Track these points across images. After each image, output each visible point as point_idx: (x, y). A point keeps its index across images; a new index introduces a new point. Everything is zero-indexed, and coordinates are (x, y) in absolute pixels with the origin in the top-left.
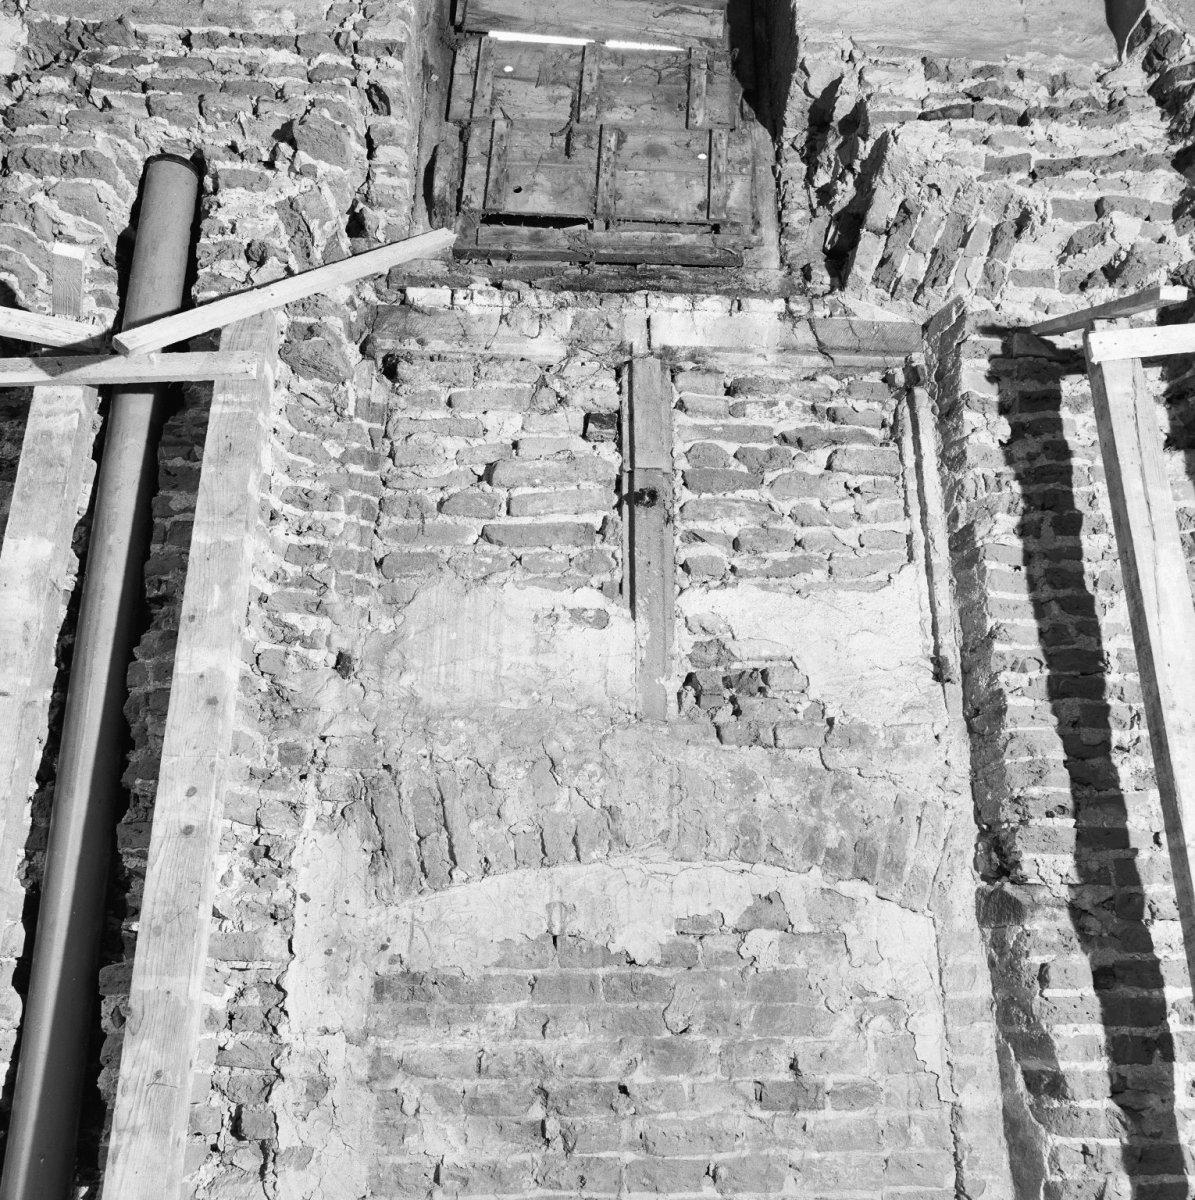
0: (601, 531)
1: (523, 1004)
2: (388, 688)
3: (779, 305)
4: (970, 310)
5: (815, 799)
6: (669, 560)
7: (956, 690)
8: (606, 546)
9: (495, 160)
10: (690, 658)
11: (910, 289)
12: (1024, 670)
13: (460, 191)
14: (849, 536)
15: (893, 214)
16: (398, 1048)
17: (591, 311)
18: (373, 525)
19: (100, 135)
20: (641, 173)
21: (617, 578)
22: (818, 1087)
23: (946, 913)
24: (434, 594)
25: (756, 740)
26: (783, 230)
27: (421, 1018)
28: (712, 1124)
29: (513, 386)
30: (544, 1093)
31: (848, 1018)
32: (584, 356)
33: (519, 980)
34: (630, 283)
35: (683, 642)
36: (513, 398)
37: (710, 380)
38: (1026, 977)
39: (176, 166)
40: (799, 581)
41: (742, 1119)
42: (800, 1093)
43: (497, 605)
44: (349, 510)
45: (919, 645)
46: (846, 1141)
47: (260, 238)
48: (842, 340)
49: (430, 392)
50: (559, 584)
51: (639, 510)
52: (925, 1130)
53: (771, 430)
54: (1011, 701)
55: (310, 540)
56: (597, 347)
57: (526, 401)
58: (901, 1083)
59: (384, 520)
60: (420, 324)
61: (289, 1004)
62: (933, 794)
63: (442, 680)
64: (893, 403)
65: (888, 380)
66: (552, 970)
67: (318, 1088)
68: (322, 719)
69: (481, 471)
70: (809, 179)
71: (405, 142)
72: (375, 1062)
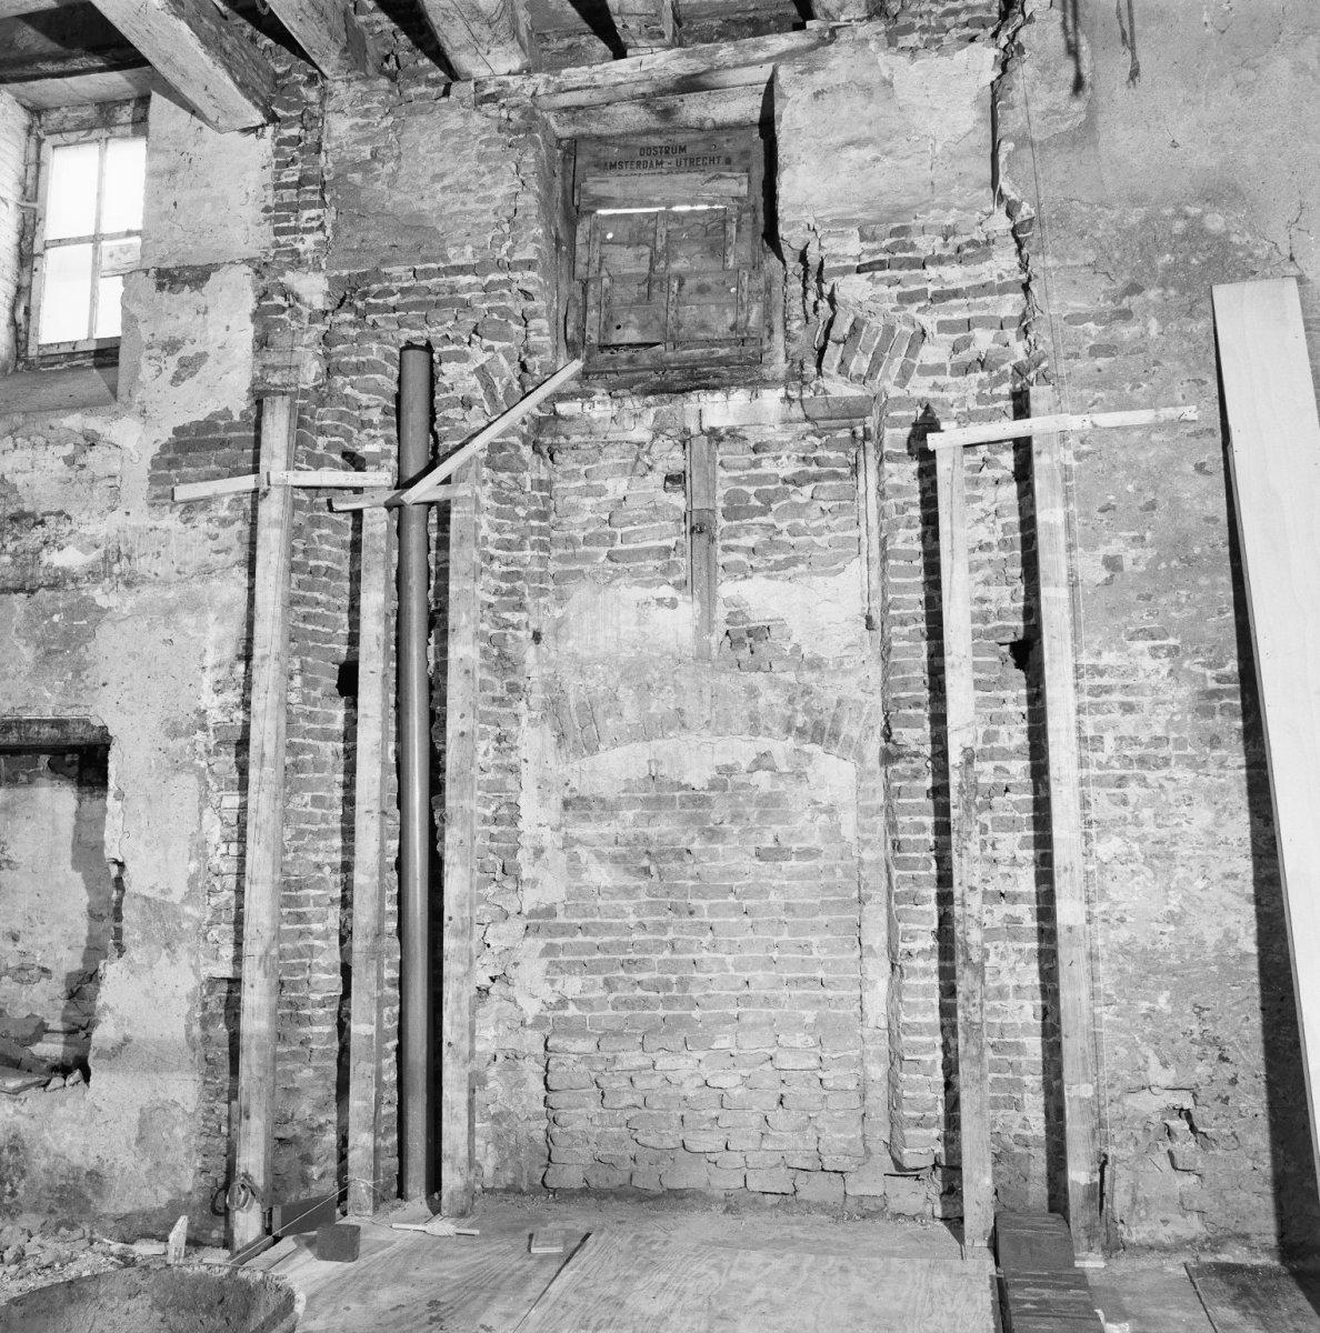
1: (638, 811)
3: (781, 392)
5: (791, 701)
15: (846, 330)
16: (576, 832)
19: (375, 346)
22: (789, 850)
23: (861, 759)
24: (580, 593)
26: (788, 337)
27: (586, 818)
32: (663, 437)
34: (691, 384)
35: (721, 613)
36: (622, 469)
37: (739, 447)
40: (790, 571)
41: (751, 864)
42: (774, 854)
43: (618, 598)
46: (801, 876)
50: (648, 584)
54: (894, 644)
57: (629, 470)
60: (564, 427)
62: (860, 696)
66: (653, 794)
68: (527, 667)
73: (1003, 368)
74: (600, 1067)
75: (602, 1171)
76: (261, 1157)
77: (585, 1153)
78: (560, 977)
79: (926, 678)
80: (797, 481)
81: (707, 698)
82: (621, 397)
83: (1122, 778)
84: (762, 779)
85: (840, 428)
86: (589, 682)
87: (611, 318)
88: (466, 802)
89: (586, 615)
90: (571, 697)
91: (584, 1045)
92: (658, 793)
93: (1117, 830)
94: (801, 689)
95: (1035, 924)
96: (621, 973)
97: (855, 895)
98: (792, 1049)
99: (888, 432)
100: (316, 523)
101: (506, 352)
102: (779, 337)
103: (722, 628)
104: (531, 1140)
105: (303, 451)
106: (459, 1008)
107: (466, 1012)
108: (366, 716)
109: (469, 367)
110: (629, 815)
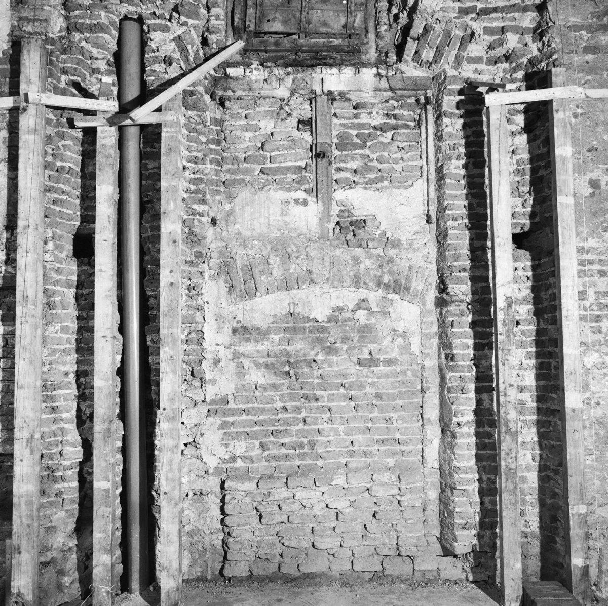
0: (305, 168)
1: (281, 335)
2: (230, 230)
3: (375, 70)
4: (448, 75)
5: (380, 266)
6: (330, 179)
7: (434, 226)
8: (307, 174)
9: (258, 8)
10: (338, 216)
11: (426, 64)
12: (456, 220)
13: (245, 22)
14: (398, 167)
15: (420, 32)
16: (241, 349)
17: (299, 76)
18: (220, 168)
19: (103, 14)
20: (319, 11)
21: (311, 186)
22: (378, 360)
23: (424, 304)
24: (243, 195)
25: (360, 246)
26: (378, 35)
27: (248, 340)
28: (344, 371)
29: (270, 109)
30: (288, 362)
31: (389, 338)
32: (297, 95)
33: (280, 327)
34: (315, 62)
35: (335, 210)
36: (270, 114)
37: (347, 104)
38: (447, 325)
39: (132, 22)
40: (379, 186)
41: (354, 369)
42: (372, 362)
43: (268, 198)
44: (211, 163)
45: (421, 209)
46: (386, 376)
47: (169, 54)
48: (399, 85)
49: (238, 113)
50: (289, 190)
51: (319, 160)
52: (412, 372)
53: (370, 124)
54: (450, 232)
55: (198, 176)
56: (302, 92)
57: (275, 115)
58: (406, 358)
59: (224, 166)
60: (232, 84)
61: (205, 336)
62: (423, 264)
63: (249, 226)
64: (418, 111)
65: (417, 101)
66: (291, 324)
67: (217, 362)
68: (208, 241)
69: (260, 145)
70: (389, 10)
71: (222, 5)
72: (234, 353)
73: (521, 60)
74: (260, 499)
75: (261, 564)
76: (30, 580)
77: (250, 554)
78: (231, 443)
79: (469, 252)
80: (382, 129)
81: (327, 264)
82: (270, 68)
83: (598, 317)
84: (361, 315)
85: (409, 97)
86: (250, 252)
87: (263, 14)
88: (174, 331)
89: (248, 208)
90: (238, 262)
91: (250, 486)
92: (293, 324)
93: (596, 348)
94: (386, 259)
95: (535, 405)
96: (272, 439)
97: (419, 387)
98: (382, 484)
99: (446, 98)
100: (62, 136)
101: (196, 27)
102: (372, 36)
103: (335, 219)
104: (213, 546)
105: (50, 82)
106: (171, 469)
107: (176, 472)
108: (101, 271)
109: (170, 36)
110: (276, 338)
